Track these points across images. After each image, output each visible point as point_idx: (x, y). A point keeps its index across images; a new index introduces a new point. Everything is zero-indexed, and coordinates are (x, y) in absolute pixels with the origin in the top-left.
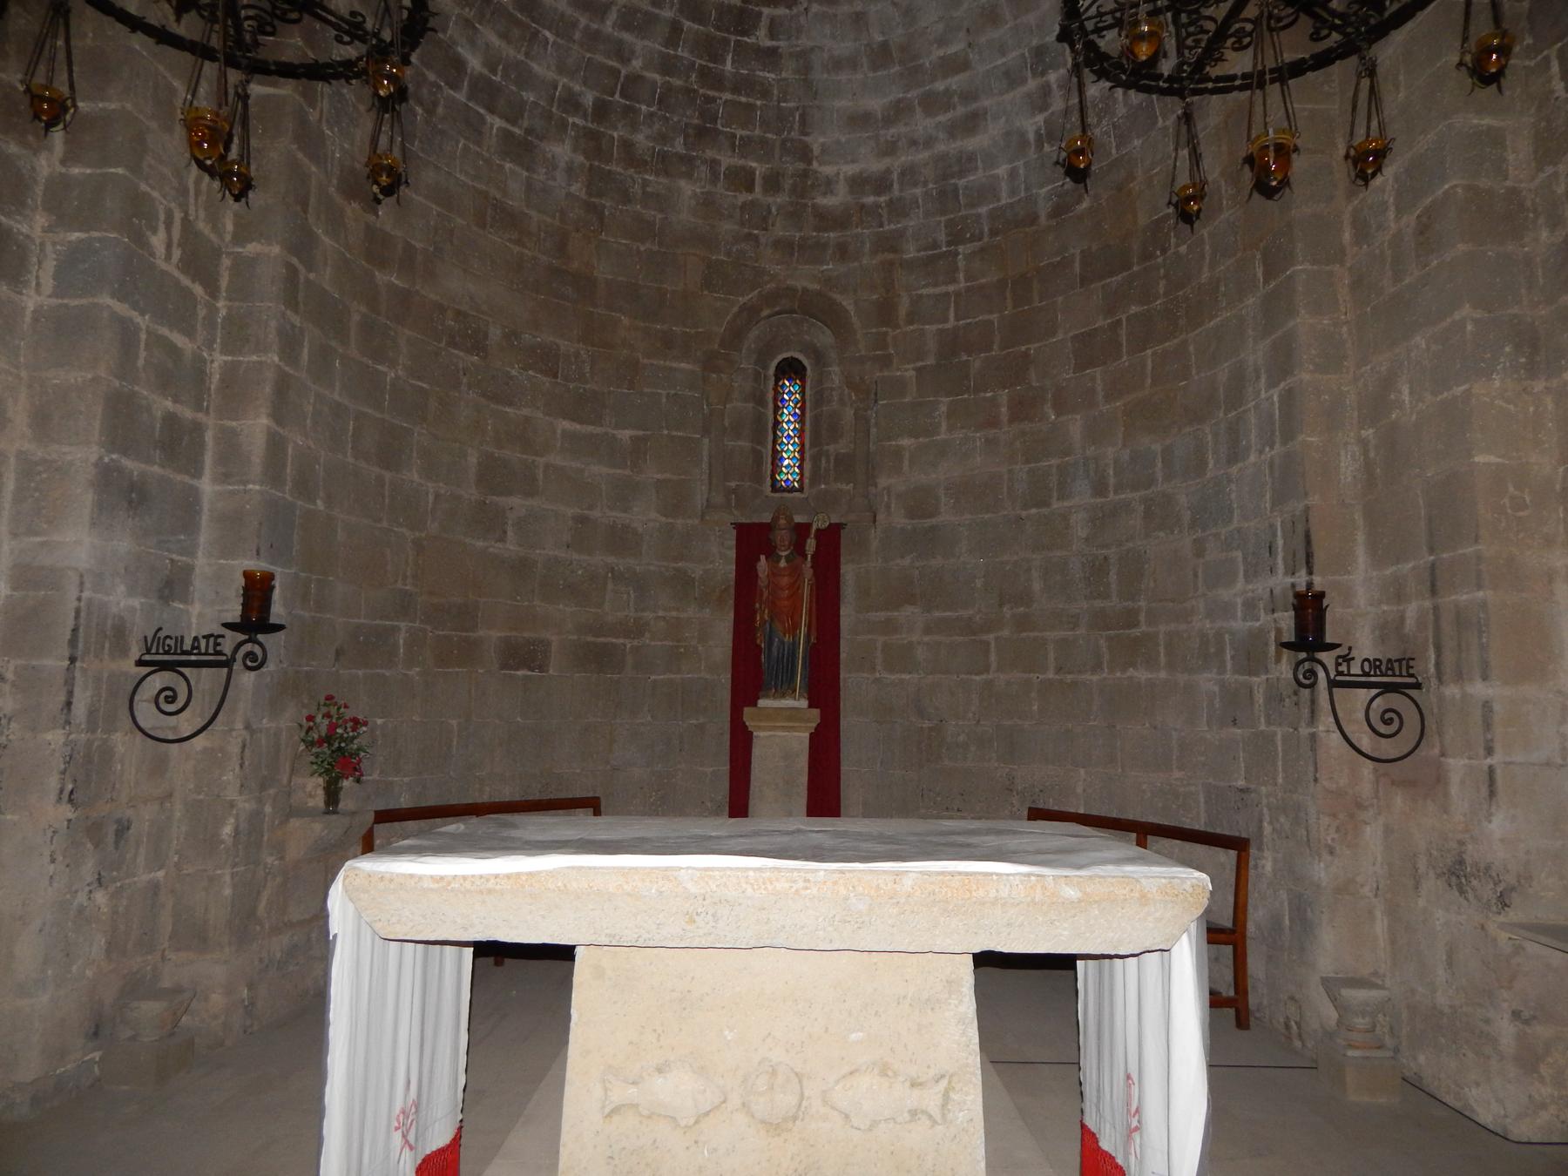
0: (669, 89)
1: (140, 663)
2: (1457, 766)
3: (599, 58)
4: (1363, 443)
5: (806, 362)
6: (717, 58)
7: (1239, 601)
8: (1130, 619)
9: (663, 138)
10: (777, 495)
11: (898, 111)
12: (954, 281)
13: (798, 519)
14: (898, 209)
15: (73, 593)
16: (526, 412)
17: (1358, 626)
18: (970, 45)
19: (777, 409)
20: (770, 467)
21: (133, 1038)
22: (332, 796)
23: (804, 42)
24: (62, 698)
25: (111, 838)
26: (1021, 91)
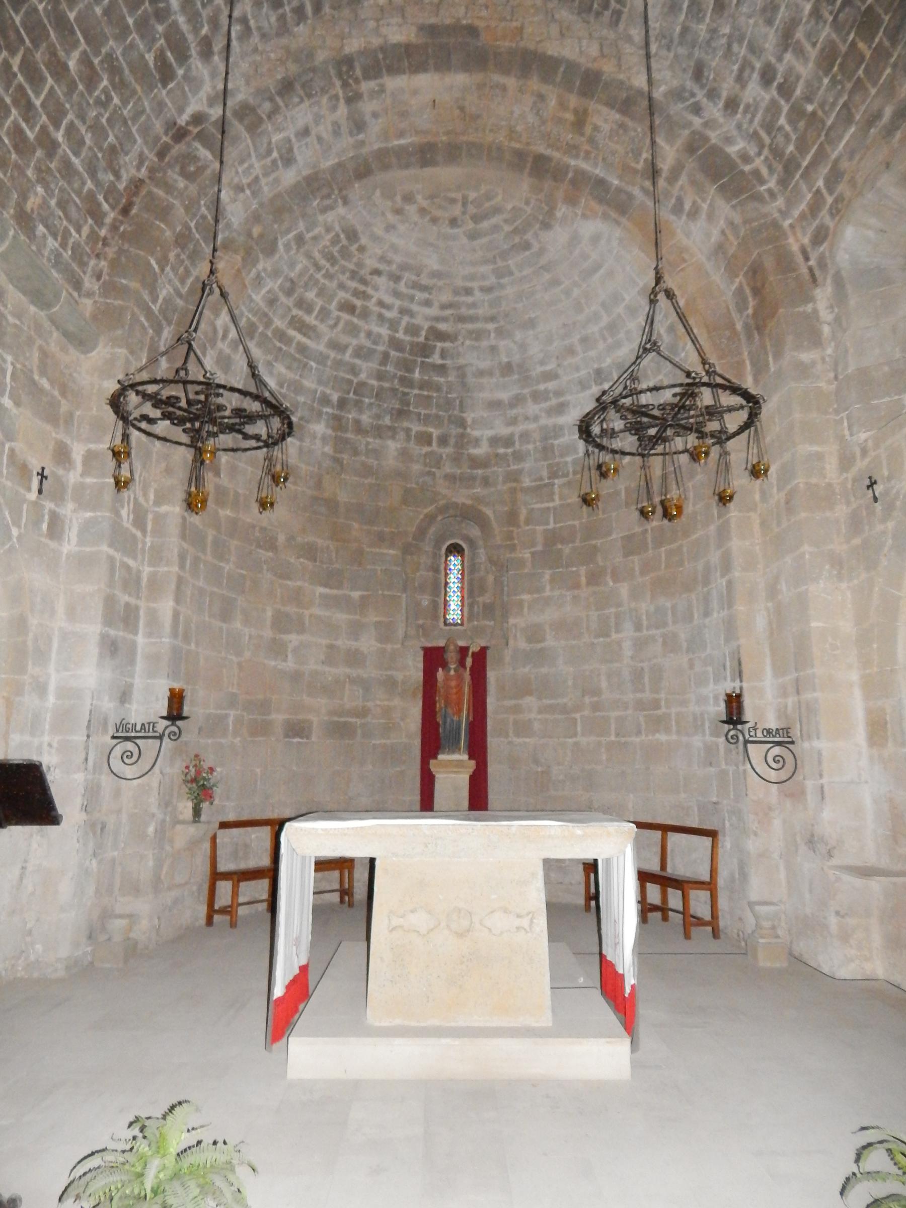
0: (381, 388)
1: (114, 737)
2: (810, 784)
3: (342, 374)
4: (767, 609)
5: (464, 546)
6: (410, 370)
7: (711, 695)
8: (656, 704)
9: (378, 417)
10: (448, 628)
11: (517, 401)
12: (553, 500)
13: (461, 643)
14: (519, 457)
15: (88, 701)
16: (299, 583)
17: (762, 711)
18: (559, 365)
19: (446, 575)
20: (442, 610)
21: (109, 939)
22: (197, 812)
23: (462, 361)
24: (84, 757)
25: (99, 831)
26: (588, 393)
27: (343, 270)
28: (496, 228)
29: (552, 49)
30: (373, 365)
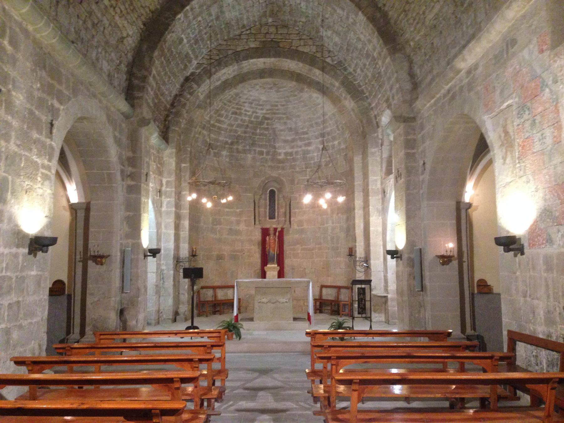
9: (244, 146)
11: (294, 140)
13: (274, 226)
14: (294, 160)
23: (274, 126)
27: (234, 103)
28: (285, 90)
29: (301, 49)
30: (243, 129)
